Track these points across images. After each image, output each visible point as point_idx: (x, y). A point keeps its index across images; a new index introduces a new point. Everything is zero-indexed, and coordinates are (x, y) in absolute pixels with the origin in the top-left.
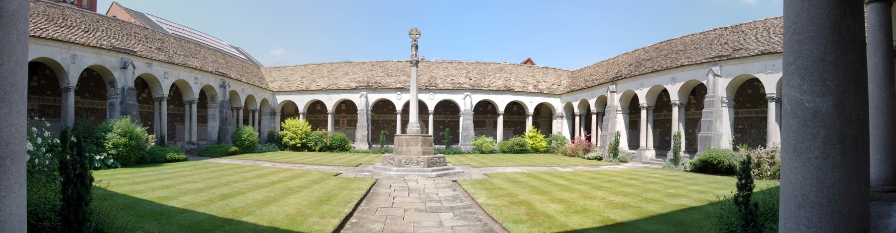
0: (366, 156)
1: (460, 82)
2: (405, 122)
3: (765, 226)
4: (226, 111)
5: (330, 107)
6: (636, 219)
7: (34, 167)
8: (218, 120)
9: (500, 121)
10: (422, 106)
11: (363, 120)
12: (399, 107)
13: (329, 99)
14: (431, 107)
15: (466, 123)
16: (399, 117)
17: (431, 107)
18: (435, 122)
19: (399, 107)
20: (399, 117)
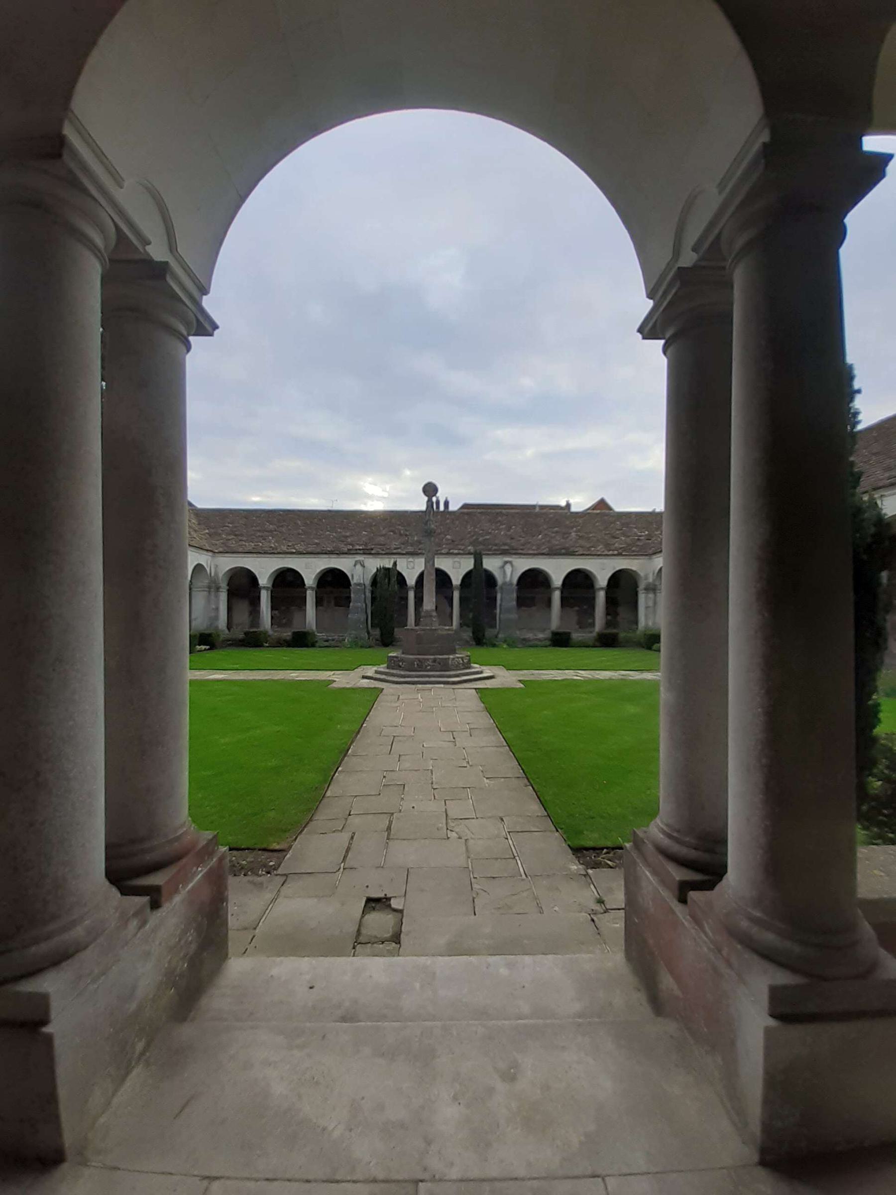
0: (373, 667)
1: (497, 542)
2: (419, 601)
3: (354, 643)
4: (251, 545)
5: (310, 579)
6: (296, 649)
7: (247, 540)
8: (492, 959)
9: (557, 596)
10: (442, 578)
11: (360, 602)
12: (411, 581)
13: (307, 567)
14: (456, 580)
15: (506, 600)
16: (411, 595)
17: (456, 580)
18: (461, 599)
19: (411, 581)
20: (411, 595)
